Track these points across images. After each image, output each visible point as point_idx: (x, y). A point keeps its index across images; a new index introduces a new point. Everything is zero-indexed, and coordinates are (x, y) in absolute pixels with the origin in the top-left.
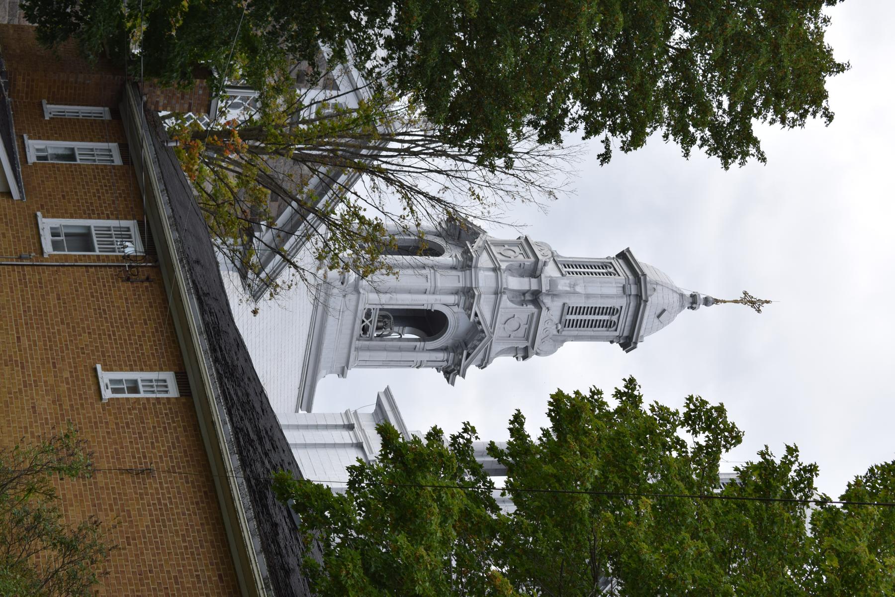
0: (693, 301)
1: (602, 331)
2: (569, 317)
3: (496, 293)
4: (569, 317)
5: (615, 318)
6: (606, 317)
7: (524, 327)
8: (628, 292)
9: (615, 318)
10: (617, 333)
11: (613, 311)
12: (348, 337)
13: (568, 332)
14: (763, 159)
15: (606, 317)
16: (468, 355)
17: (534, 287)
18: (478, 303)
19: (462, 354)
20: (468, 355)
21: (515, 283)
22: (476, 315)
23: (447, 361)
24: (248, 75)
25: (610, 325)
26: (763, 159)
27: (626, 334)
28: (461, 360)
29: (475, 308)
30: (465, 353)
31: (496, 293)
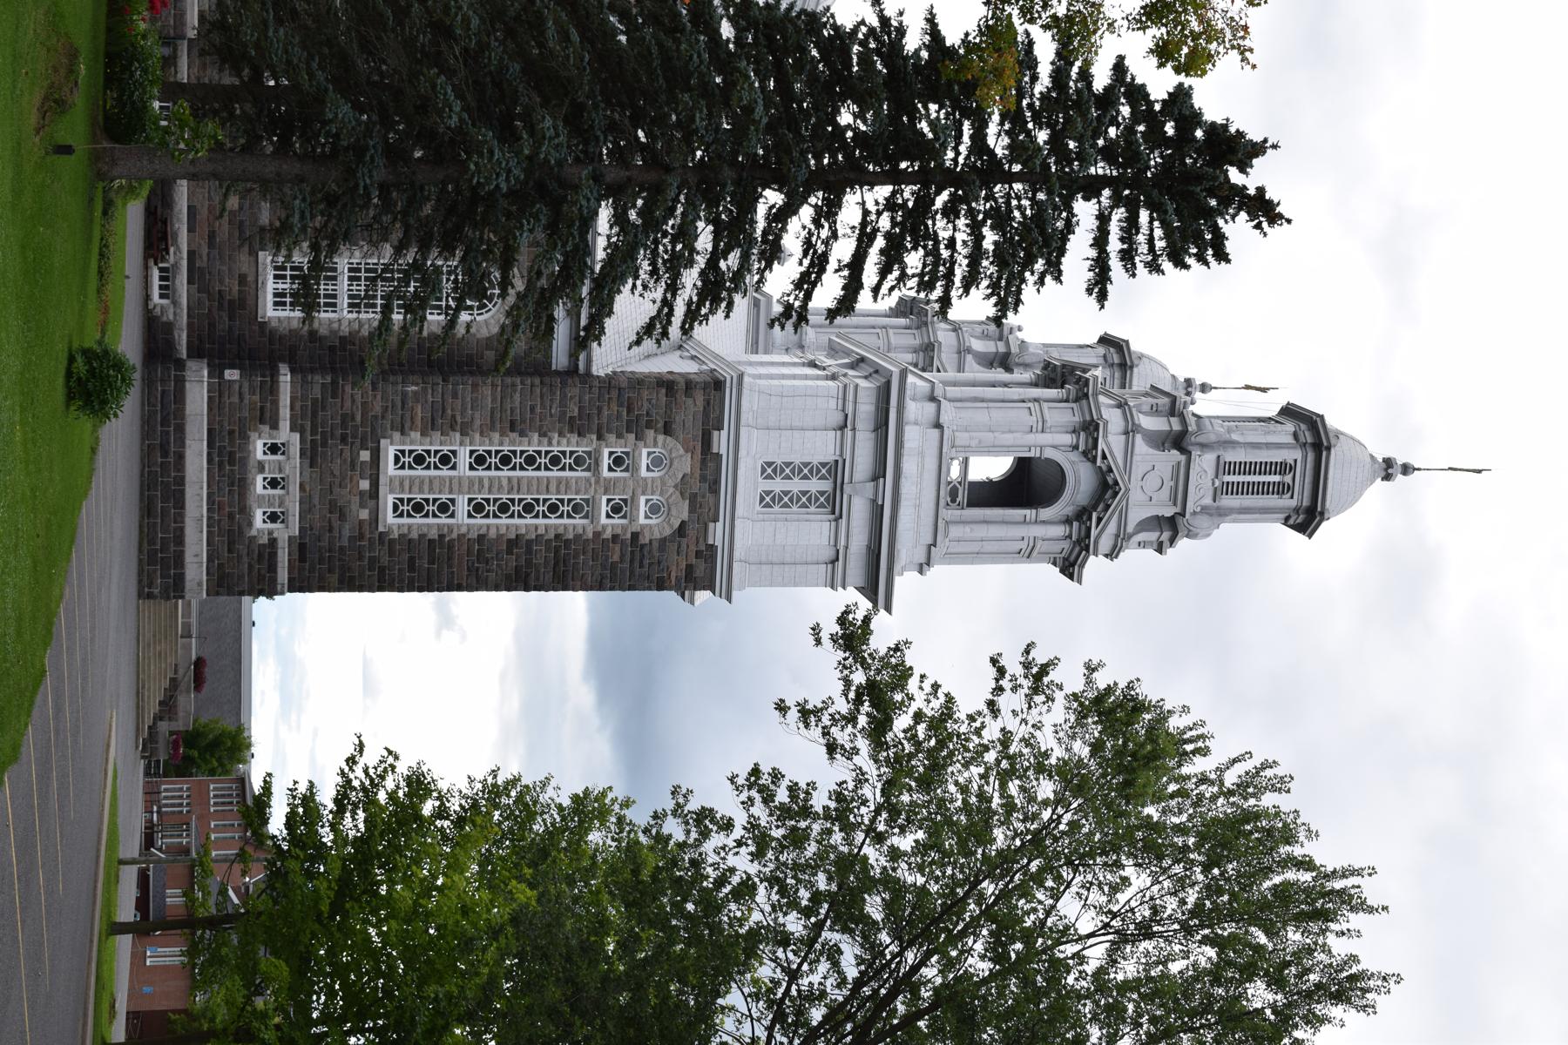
0: (1388, 470)
1: (1272, 501)
2: (1227, 478)
3: (1126, 433)
4: (1227, 478)
5: (1288, 479)
6: (1277, 478)
7: (1169, 484)
8: (1302, 439)
9: (1288, 479)
10: (1293, 503)
11: (1283, 468)
12: (932, 505)
13: (1228, 501)
14: (1373, 872)
15: (1277, 478)
16: (1099, 520)
17: (1177, 427)
18: (1105, 436)
19: (1090, 519)
20: (1099, 520)
21: (1149, 423)
22: (1104, 457)
23: (1070, 537)
24: (531, 817)
25: (1282, 489)
26: (1373, 872)
27: (1306, 503)
28: (1089, 529)
29: (1101, 445)
30: (1094, 515)
31: (1126, 433)
